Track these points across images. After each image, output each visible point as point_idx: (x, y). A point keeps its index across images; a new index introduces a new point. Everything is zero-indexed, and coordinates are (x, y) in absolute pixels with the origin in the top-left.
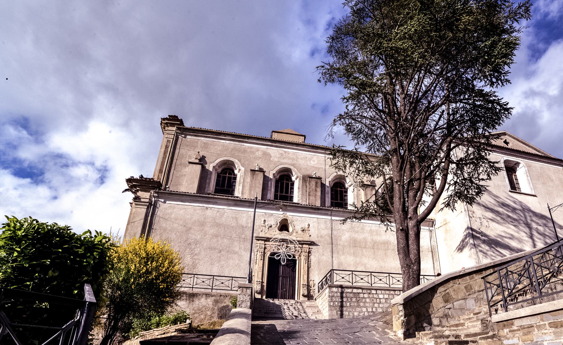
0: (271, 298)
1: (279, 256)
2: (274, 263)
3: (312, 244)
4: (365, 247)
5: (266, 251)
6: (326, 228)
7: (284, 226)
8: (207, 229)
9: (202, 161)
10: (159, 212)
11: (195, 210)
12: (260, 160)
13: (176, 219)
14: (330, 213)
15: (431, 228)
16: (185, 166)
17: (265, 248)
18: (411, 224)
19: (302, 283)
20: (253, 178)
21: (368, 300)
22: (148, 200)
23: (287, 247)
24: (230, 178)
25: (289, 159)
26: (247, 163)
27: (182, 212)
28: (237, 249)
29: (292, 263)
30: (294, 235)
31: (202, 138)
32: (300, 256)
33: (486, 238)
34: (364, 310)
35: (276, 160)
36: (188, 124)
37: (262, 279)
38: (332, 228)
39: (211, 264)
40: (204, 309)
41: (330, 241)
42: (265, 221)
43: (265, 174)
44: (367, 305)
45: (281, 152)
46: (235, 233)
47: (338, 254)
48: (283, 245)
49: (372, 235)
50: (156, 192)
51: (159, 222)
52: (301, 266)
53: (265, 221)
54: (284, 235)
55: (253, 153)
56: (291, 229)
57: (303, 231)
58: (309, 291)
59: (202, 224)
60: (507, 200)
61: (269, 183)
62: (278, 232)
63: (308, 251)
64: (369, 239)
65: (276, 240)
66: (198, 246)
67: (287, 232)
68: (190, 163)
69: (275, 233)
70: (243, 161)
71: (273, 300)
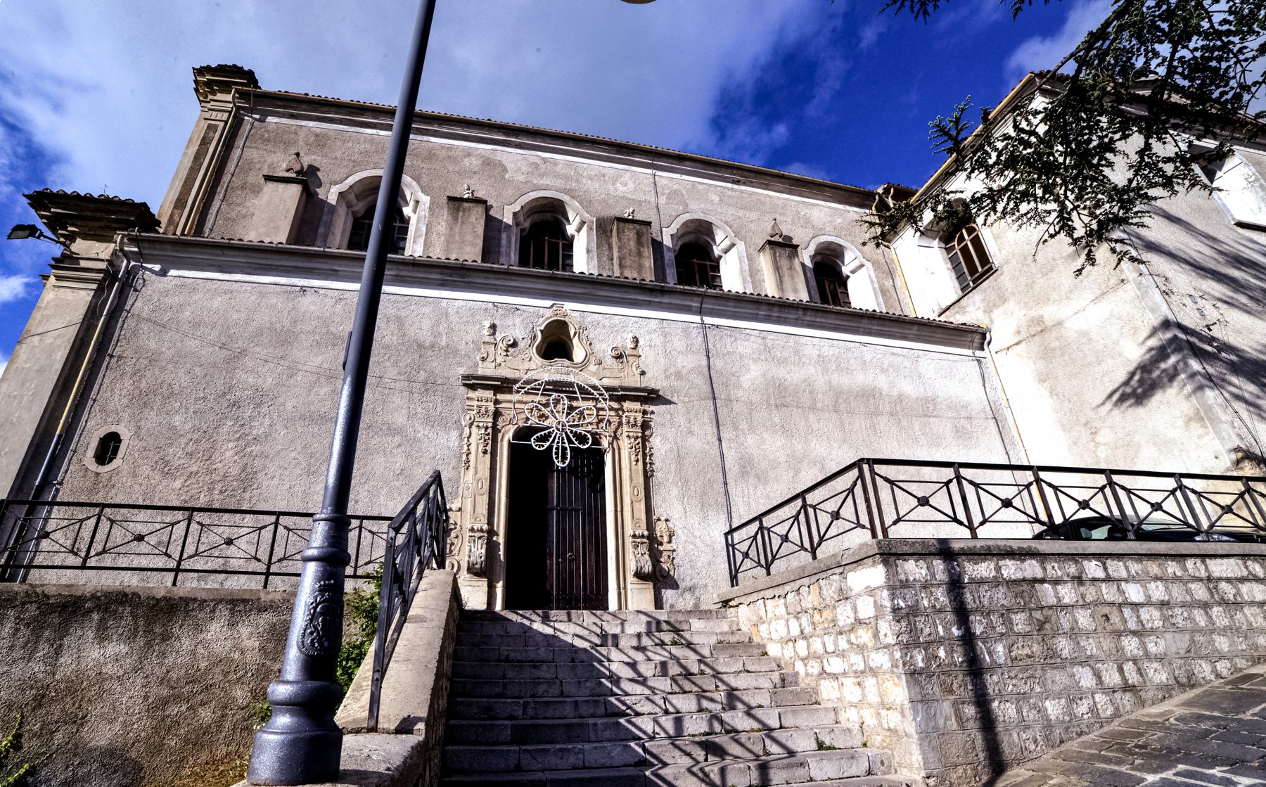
0: (533, 608)
1: (544, 439)
2: (528, 465)
3: (651, 397)
4: (813, 408)
5: (500, 423)
6: (689, 349)
7: (556, 343)
8: (298, 353)
9: (307, 179)
10: (139, 304)
11: (262, 295)
12: (476, 177)
13: (197, 325)
15: (978, 353)
16: (257, 190)
17: (497, 414)
19: (629, 531)
20: (456, 219)
22: (103, 266)
23: (571, 408)
25: (557, 176)
26: (436, 185)
27: (217, 302)
28: (400, 419)
29: (589, 462)
30: (590, 364)
31: (311, 124)
32: (615, 438)
33: (1137, 377)
35: (522, 178)
36: (268, 84)
38: (708, 350)
39: (309, 473)
41: (706, 388)
42: (493, 327)
43: (492, 213)
44: (1090, 646)
45: (533, 160)
46: (396, 364)
47: (736, 428)
48: (557, 402)
49: (825, 371)
50: (133, 240)
51: (135, 333)
52: (621, 471)
55: (455, 160)
56: (578, 353)
58: (655, 555)
59: (284, 338)
60: (1247, 251)
61: (504, 236)
62: (538, 360)
63: (640, 420)
64: (820, 382)
65: (532, 387)
66: (264, 409)
67: (567, 362)
69: (527, 365)
70: (425, 179)
71: (546, 619)
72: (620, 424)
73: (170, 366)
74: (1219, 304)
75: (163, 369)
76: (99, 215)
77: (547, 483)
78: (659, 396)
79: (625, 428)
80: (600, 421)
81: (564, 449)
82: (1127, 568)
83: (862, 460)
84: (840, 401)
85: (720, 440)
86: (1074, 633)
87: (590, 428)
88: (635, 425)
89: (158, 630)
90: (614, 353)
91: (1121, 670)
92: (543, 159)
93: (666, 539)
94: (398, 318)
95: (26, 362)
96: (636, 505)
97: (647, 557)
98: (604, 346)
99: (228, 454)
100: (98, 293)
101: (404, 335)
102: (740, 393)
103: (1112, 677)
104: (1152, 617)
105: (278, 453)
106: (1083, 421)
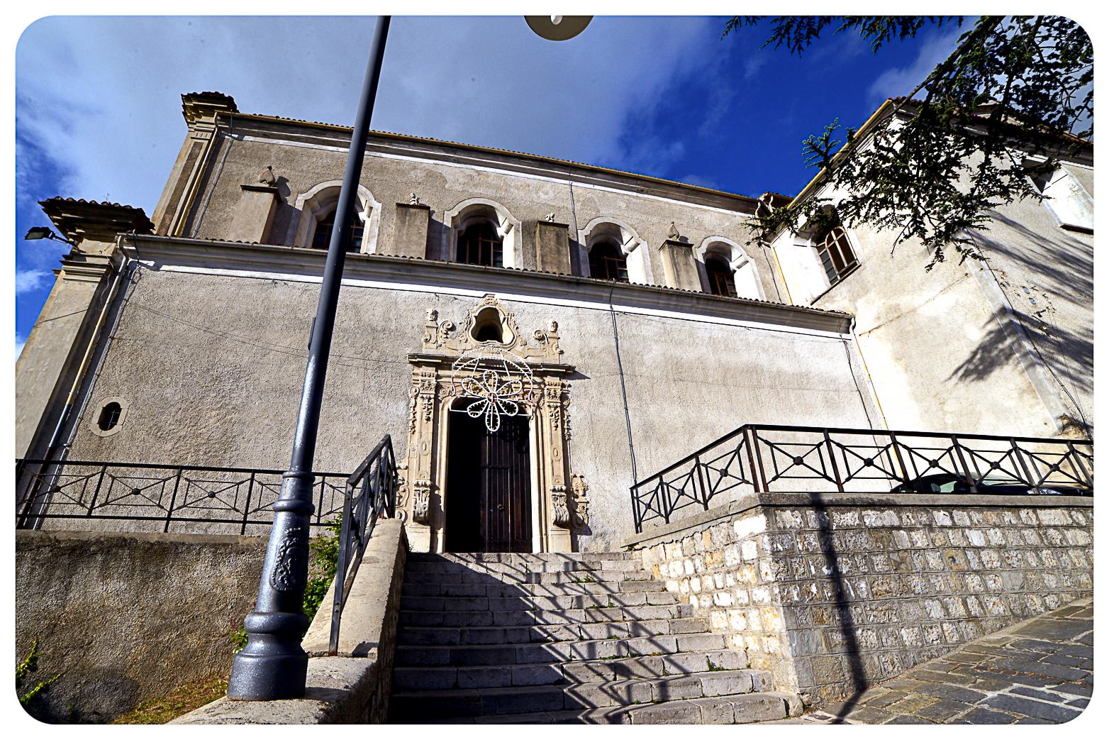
0: (468, 550)
1: (478, 408)
2: (465, 431)
3: (569, 373)
4: (705, 382)
5: (441, 395)
7: (488, 328)
8: (269, 336)
9: (278, 189)
10: (136, 294)
11: (240, 287)
12: (421, 187)
15: (844, 336)
17: (438, 387)
19: (550, 486)
20: (403, 222)
21: (933, 560)
22: (106, 262)
23: (501, 382)
25: (489, 186)
27: (202, 293)
28: (356, 391)
29: (516, 428)
30: (518, 344)
31: (281, 142)
32: (538, 407)
35: (459, 188)
36: (244, 109)
37: (433, 478)
40: (201, 609)
42: (435, 313)
43: (433, 217)
44: (939, 584)
45: (468, 172)
46: (353, 345)
48: (489, 377)
50: (131, 240)
53: (435, 313)
54: (487, 351)
55: (403, 173)
56: (507, 336)
57: (541, 339)
58: (572, 507)
59: (259, 323)
60: (1072, 249)
61: (444, 236)
63: (559, 392)
64: (711, 359)
65: (467, 364)
66: (242, 383)
67: (497, 343)
68: (245, 188)
69: (463, 346)
70: (377, 189)
71: (479, 561)
72: (542, 395)
74: (1048, 294)
75: (156, 349)
76: (102, 219)
79: (547, 399)
80: (526, 393)
81: (495, 417)
82: (970, 517)
83: (746, 426)
84: (728, 376)
85: (626, 409)
86: (926, 572)
87: (516, 399)
91: (965, 603)
92: (477, 171)
93: (581, 493)
94: (355, 306)
97: (565, 507)
103: (958, 610)
105: (254, 420)
106: (933, 393)
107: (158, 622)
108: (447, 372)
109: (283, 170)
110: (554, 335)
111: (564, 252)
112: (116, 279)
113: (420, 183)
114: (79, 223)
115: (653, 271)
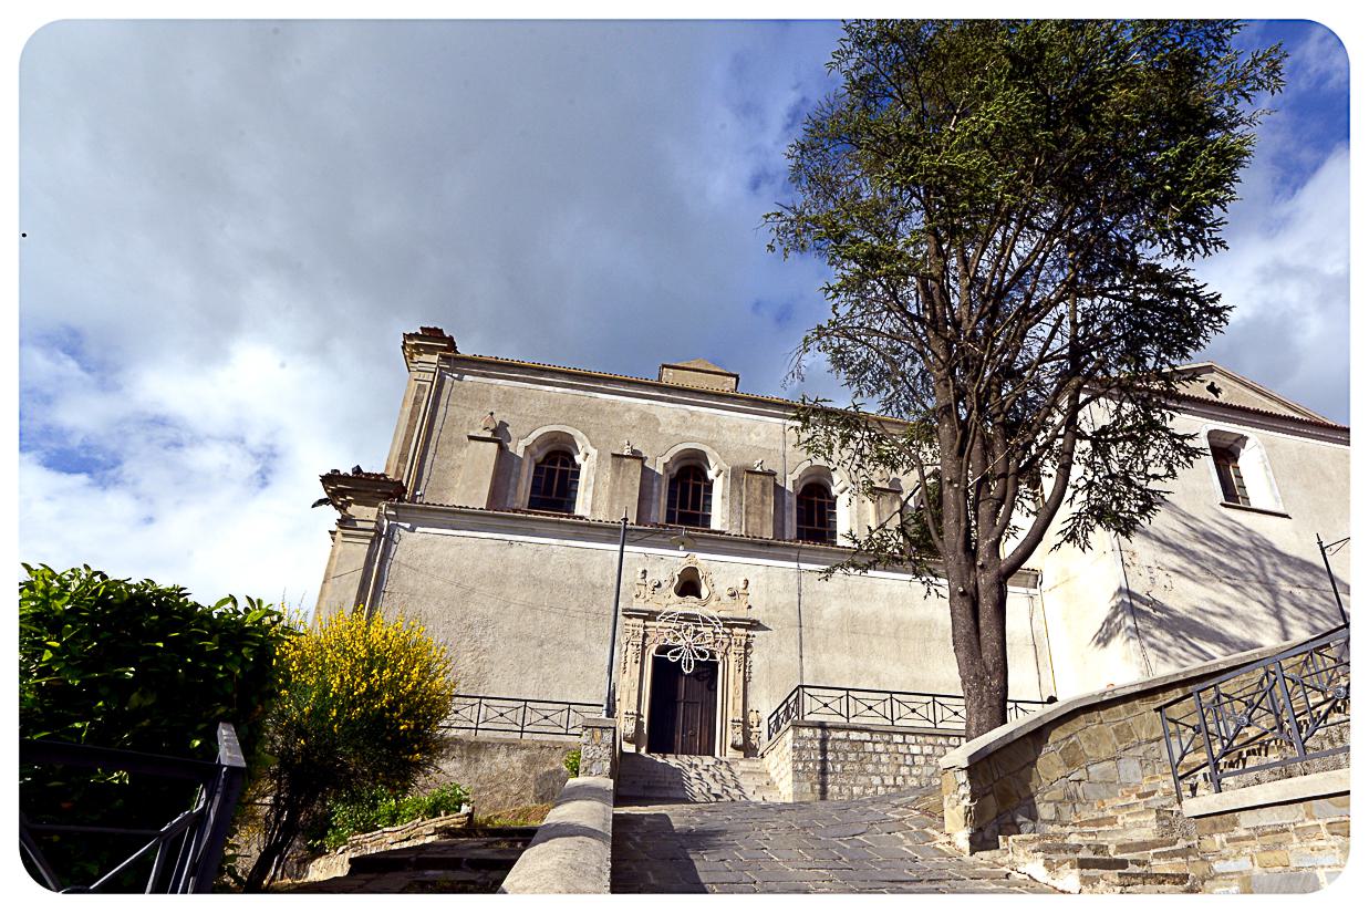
1: (677, 653)
2: (665, 673)
3: (755, 625)
4: (877, 634)
5: (647, 642)
7: (689, 585)
9: (499, 435)
10: (400, 553)
13: (439, 570)
14: (794, 554)
15: (1032, 591)
16: (461, 446)
17: (645, 636)
18: (985, 580)
19: (730, 718)
20: (618, 473)
21: (884, 758)
22: (372, 526)
23: (696, 632)
24: (564, 474)
27: (451, 552)
28: (580, 639)
31: (500, 382)
32: (726, 654)
34: (876, 780)
35: (672, 431)
36: (464, 350)
37: (639, 709)
38: (800, 590)
39: (521, 674)
42: (645, 572)
43: (646, 464)
46: (577, 599)
48: (687, 627)
50: (391, 507)
53: (645, 572)
54: (689, 605)
55: (617, 415)
56: (704, 592)
58: (746, 735)
59: (500, 580)
60: (1217, 526)
61: (656, 485)
63: (744, 642)
67: (696, 599)
68: (471, 438)
70: (593, 433)
71: (664, 758)
72: (730, 644)
73: (424, 599)
74: (1171, 573)
75: (419, 601)
76: (369, 489)
77: (677, 683)
78: (759, 624)
79: (733, 646)
80: (717, 642)
81: (690, 661)
84: (901, 629)
85: (801, 657)
87: (708, 647)
88: (740, 645)
89: (473, 756)
90: (730, 592)
91: (895, 779)
92: (691, 412)
93: (755, 724)
94: (578, 565)
95: (332, 596)
96: (736, 700)
97: (740, 735)
98: (723, 587)
99: (467, 661)
100: (371, 545)
101: (582, 578)
102: (821, 623)
104: (920, 760)
105: (500, 661)
107: (479, 786)
108: (653, 624)
109: (503, 414)
110: (745, 592)
111: (768, 502)
112: (382, 541)
113: (634, 427)
114: (349, 492)
115: (858, 516)
